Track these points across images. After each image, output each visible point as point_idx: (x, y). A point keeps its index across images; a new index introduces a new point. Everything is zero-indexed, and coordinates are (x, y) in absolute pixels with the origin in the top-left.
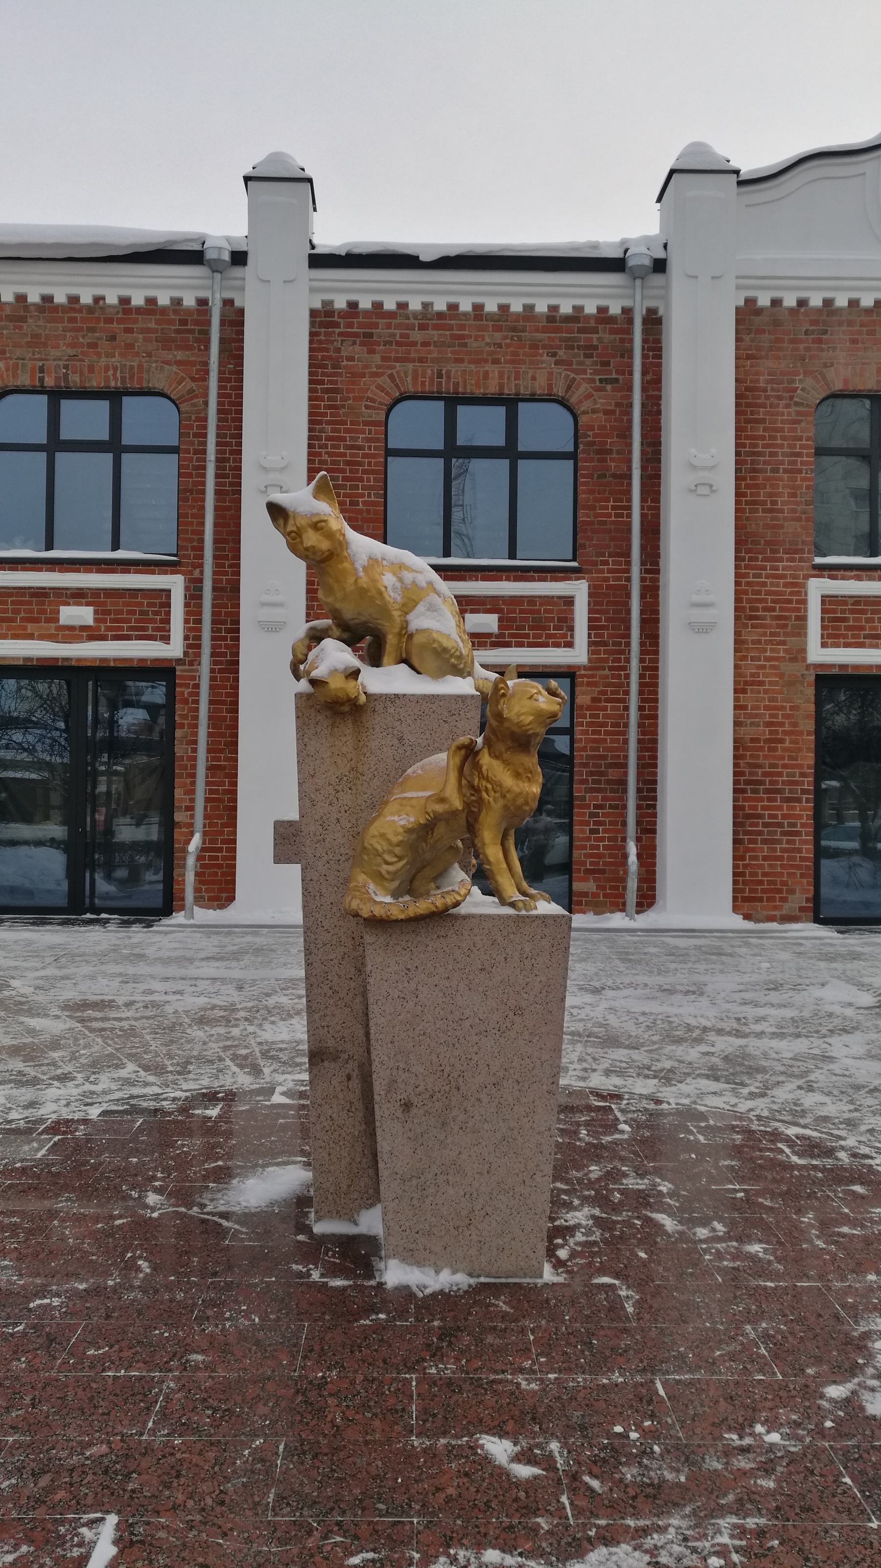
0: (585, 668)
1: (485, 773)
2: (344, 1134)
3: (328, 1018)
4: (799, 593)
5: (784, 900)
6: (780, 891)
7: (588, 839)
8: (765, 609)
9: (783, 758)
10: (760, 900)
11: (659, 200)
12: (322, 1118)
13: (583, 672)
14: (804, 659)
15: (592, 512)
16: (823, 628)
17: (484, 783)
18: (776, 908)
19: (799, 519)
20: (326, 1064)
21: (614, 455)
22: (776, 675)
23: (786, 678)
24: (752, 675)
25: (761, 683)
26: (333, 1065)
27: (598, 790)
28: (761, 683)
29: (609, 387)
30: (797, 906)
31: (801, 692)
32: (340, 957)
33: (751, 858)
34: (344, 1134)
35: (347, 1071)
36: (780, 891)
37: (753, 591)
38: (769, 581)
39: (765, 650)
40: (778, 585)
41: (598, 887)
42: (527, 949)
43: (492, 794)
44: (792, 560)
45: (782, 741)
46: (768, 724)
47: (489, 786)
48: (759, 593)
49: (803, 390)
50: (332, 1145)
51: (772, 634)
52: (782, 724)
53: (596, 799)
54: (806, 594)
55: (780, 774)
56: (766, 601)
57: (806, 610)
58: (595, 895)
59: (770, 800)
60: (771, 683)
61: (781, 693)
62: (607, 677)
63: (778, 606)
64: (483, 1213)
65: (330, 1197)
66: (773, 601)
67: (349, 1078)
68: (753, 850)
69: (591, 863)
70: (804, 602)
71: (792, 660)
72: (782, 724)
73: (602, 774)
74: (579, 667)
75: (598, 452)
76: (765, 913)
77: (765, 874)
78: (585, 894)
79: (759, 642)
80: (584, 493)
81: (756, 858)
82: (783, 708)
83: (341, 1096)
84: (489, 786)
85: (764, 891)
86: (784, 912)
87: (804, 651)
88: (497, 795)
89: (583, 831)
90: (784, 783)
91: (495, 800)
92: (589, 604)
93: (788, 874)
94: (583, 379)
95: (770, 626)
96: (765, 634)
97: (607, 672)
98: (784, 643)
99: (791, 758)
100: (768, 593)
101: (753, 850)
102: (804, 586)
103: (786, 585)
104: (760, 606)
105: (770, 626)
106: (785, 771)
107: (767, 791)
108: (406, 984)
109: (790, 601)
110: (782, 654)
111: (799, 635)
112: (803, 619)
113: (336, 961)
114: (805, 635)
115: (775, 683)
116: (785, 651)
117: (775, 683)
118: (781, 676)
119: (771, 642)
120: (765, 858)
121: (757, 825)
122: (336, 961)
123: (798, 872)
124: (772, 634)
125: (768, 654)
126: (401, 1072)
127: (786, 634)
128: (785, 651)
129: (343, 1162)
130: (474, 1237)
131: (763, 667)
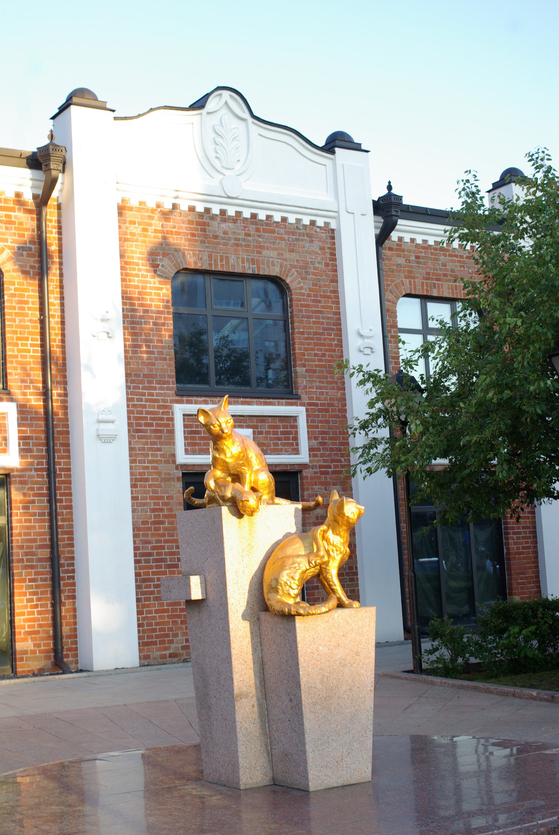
0: (18, 470)
1: (332, 543)
2: (252, 736)
3: (243, 676)
4: (168, 413)
5: (171, 642)
6: (167, 636)
7: (26, 607)
8: (147, 425)
9: (164, 535)
10: (155, 643)
11: (53, 118)
12: (242, 729)
13: (15, 473)
14: (174, 462)
15: (16, 348)
16: (186, 438)
17: (331, 547)
18: (166, 649)
19: (165, 359)
20: (243, 700)
21: (30, 305)
22: (156, 473)
23: (163, 476)
24: (140, 474)
25: (147, 480)
26: (246, 700)
27: (32, 567)
28: (147, 480)
29: (25, 253)
30: (180, 645)
31: (174, 485)
32: (247, 644)
33: (148, 612)
34: (252, 736)
35: (252, 703)
36: (167, 636)
37: (137, 411)
38: (147, 404)
39: (147, 455)
40: (154, 407)
41: (35, 645)
42: (360, 624)
43: (335, 552)
44: (162, 389)
45: (162, 523)
46: (153, 510)
47: (334, 549)
48: (141, 412)
49: (163, 266)
50: (247, 743)
51: (152, 443)
52: (162, 510)
53: (30, 573)
54: (173, 414)
55: (163, 548)
56: (146, 418)
57: (173, 425)
58: (33, 652)
59: (157, 567)
60: (153, 480)
61: (161, 487)
62: (33, 476)
63: (154, 422)
64: (347, 753)
65: (247, 771)
66: (152, 419)
67: (253, 706)
68: (148, 606)
69: (29, 627)
70: (172, 419)
71: (167, 462)
72: (162, 510)
73: (33, 554)
74: (12, 470)
75: (19, 302)
76: (159, 653)
77: (157, 624)
78: (25, 652)
79: (143, 449)
80: (10, 333)
81: (150, 612)
82: (162, 498)
83: (250, 716)
84: (334, 549)
85: (157, 637)
86: (171, 651)
87: (174, 455)
88: (338, 552)
89: (22, 601)
90: (166, 554)
91: (337, 555)
92: (18, 420)
93: (173, 622)
94: (6, 246)
95: (150, 437)
96: (147, 443)
97: (33, 473)
98: (160, 449)
99: (169, 535)
100: (147, 413)
101: (148, 606)
102: (171, 407)
103: (159, 407)
104: (143, 422)
105: (150, 437)
106: (166, 545)
107: (156, 561)
108: (313, 646)
109: (162, 419)
110: (159, 458)
111: (170, 443)
112: (172, 432)
113: (245, 646)
114: (174, 444)
115: (156, 480)
116: (162, 456)
117: (156, 480)
118: (160, 474)
119: (151, 449)
120: (156, 611)
121: (150, 587)
122: (245, 646)
123: (179, 620)
124: (152, 443)
125: (150, 458)
126: (313, 688)
127: (161, 443)
128: (162, 456)
129: (253, 751)
130: (345, 766)
131: (147, 468)
